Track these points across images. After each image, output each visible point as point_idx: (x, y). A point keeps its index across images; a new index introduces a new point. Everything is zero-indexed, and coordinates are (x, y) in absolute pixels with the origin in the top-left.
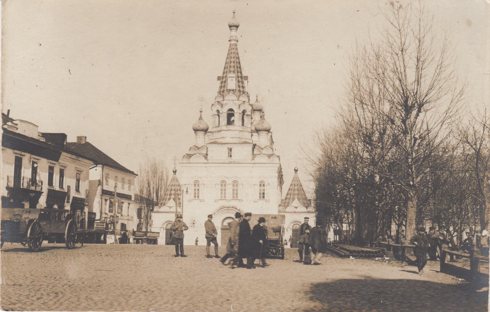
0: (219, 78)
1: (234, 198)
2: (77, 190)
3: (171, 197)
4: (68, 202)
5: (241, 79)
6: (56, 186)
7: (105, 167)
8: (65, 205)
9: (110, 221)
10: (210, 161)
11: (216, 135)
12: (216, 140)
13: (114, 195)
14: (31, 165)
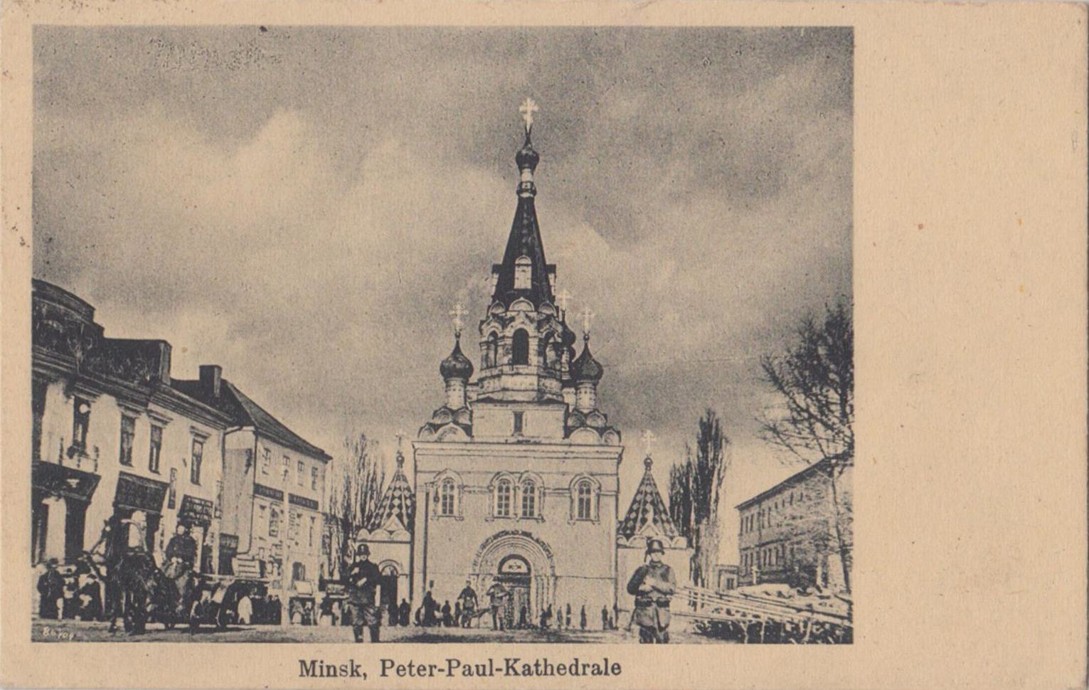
0: (496, 269)
1: (582, 516)
2: (195, 480)
3: (393, 511)
4: (171, 506)
5: (543, 271)
6: (140, 467)
7: (260, 438)
8: (162, 514)
9: (270, 556)
10: (476, 439)
11: (491, 385)
12: (491, 395)
13: (282, 499)
14: (72, 410)
